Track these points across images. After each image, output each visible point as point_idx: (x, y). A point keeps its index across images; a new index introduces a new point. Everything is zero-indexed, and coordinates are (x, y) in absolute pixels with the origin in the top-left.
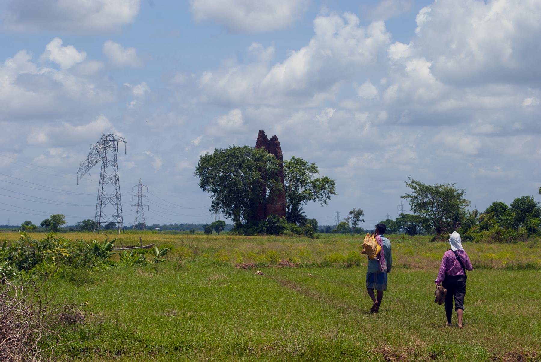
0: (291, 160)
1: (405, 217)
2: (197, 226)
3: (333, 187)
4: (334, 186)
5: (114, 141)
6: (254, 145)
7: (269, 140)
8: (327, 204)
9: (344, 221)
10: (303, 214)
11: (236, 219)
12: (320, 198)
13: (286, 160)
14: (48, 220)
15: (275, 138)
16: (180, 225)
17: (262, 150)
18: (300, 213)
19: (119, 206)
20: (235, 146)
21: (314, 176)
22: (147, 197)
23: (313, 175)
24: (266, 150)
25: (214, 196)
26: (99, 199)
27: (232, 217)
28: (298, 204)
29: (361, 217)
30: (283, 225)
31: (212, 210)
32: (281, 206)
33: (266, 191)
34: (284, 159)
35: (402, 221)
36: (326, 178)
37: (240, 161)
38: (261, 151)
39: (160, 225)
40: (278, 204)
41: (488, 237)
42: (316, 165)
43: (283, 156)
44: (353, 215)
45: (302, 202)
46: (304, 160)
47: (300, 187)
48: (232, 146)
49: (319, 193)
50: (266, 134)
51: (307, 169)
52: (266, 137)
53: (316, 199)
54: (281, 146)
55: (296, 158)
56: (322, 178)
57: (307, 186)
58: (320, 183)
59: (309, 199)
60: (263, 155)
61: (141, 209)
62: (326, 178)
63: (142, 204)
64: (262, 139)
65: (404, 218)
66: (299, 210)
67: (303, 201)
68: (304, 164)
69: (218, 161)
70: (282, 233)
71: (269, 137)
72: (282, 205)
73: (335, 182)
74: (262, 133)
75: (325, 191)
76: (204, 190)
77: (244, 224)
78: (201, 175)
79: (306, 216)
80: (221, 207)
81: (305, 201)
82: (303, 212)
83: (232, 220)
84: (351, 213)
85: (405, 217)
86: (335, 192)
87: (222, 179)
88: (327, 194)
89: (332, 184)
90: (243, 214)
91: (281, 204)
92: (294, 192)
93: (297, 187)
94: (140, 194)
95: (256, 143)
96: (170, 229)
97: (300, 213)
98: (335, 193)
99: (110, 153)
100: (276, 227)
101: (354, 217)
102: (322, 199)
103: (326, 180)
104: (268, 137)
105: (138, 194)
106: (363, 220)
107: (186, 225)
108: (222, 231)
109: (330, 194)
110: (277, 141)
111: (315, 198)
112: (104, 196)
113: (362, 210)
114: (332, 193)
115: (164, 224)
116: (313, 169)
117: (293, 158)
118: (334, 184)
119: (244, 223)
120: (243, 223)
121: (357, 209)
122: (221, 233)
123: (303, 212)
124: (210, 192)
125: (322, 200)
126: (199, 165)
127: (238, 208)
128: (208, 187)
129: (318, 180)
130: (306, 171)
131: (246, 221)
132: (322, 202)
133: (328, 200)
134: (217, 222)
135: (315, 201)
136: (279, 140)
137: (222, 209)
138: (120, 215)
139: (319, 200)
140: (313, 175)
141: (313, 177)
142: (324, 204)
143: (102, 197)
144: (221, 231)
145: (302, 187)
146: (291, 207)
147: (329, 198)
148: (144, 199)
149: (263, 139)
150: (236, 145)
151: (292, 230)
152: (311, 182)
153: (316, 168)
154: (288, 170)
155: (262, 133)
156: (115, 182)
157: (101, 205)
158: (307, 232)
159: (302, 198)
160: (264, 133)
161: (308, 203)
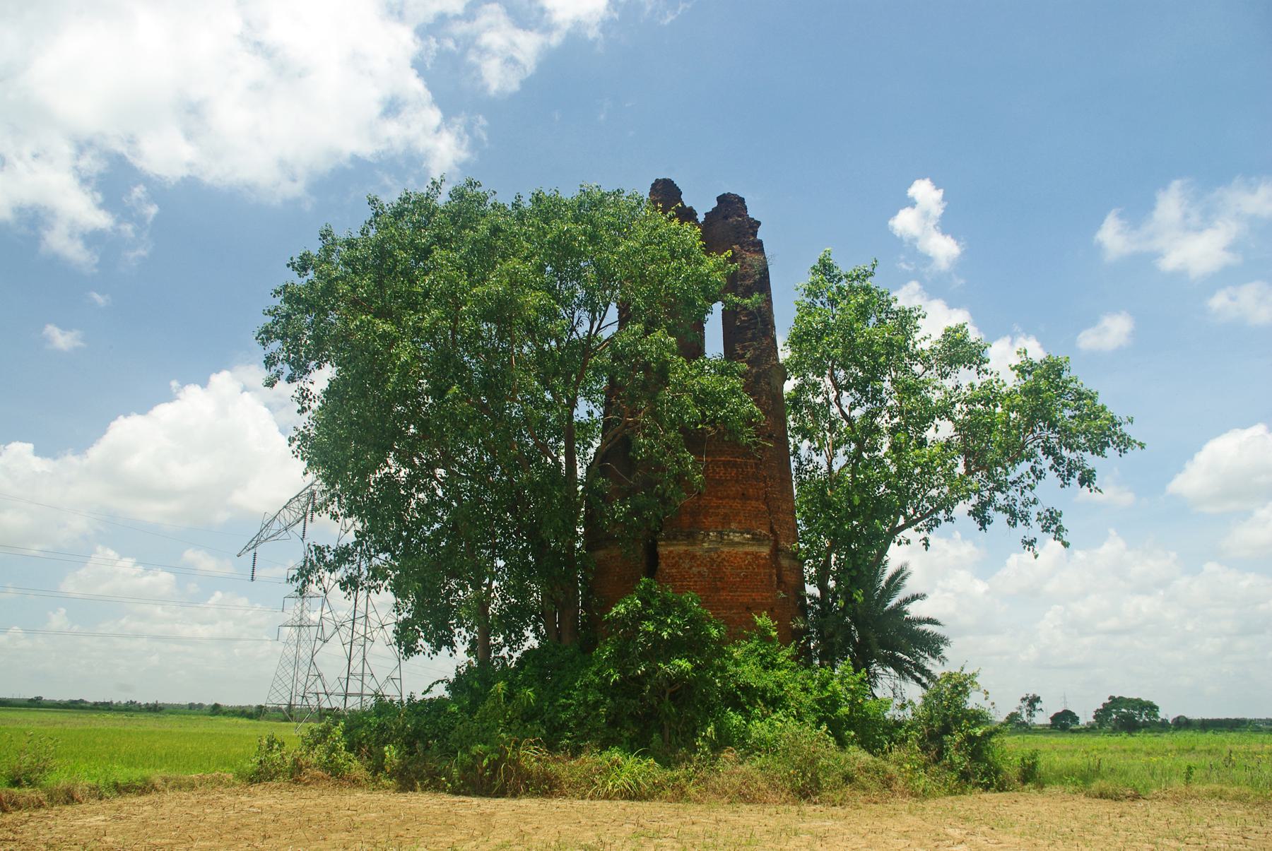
8: (1066, 545)
10: (914, 610)
18: (893, 602)
29: (1038, 706)
30: (459, 644)
32: (756, 556)
44: (1026, 703)
70: (723, 741)
72: (765, 551)
84: (1023, 700)
91: (757, 539)
97: (893, 602)
101: (1029, 705)
121: (1031, 695)
132: (1035, 529)
147: (1087, 479)
151: (826, 711)
158: (947, 730)
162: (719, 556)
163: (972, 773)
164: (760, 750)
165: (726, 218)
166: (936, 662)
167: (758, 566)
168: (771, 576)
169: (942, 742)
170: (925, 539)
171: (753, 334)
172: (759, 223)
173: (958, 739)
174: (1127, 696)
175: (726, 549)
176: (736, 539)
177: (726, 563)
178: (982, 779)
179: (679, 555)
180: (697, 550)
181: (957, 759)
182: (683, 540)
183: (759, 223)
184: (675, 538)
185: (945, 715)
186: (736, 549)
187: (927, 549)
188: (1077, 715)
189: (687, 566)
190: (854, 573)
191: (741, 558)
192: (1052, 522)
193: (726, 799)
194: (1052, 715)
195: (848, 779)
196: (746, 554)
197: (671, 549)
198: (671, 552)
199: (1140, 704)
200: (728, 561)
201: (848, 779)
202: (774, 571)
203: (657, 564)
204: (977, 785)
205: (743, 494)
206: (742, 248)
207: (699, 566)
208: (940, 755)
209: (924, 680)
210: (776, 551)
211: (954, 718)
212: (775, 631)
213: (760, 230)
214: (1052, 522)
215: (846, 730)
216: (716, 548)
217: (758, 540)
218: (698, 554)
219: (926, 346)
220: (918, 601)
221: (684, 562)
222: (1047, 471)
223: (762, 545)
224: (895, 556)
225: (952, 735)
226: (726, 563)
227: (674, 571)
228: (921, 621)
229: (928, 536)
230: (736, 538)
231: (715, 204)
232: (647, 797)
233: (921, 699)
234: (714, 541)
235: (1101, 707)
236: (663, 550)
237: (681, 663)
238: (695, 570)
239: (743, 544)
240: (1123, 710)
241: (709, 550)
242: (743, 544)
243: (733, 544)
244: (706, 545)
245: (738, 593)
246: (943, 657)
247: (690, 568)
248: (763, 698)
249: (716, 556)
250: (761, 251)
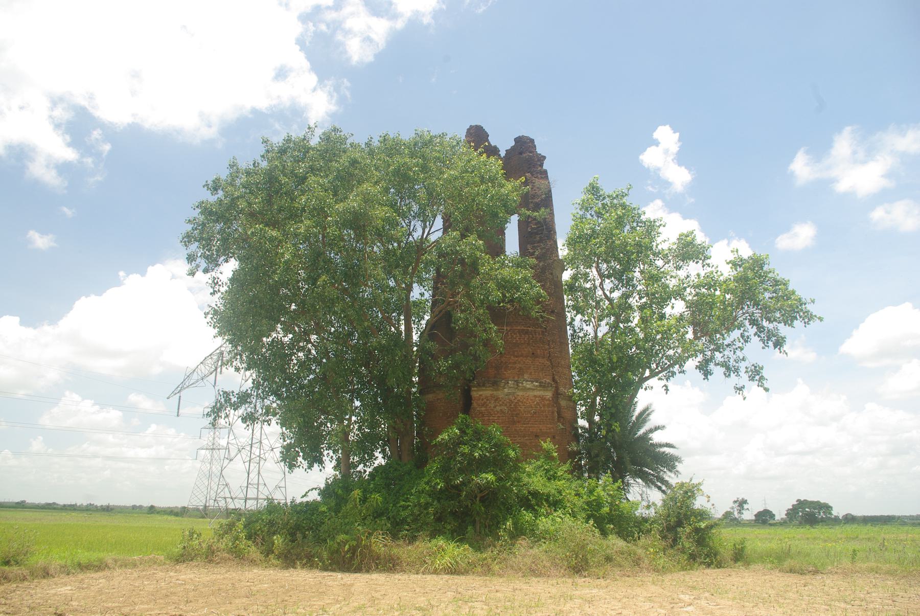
8: (767, 390)
9: (729, 510)
10: (657, 437)
16: (300, 503)
18: (641, 432)
29: (746, 506)
32: (543, 398)
41: (203, 461)
43: (552, 191)
44: (737, 504)
54: (546, 166)
72: (549, 394)
79: (668, 445)
84: (735, 502)
91: (543, 386)
97: (641, 432)
113: (746, 499)
121: (741, 499)
125: (743, 370)
131: (41, 438)
132: (744, 379)
158: (679, 524)
162: (516, 398)
163: (698, 555)
164: (545, 539)
165: (521, 153)
166: (672, 475)
167: (544, 405)
168: (553, 412)
169: (676, 533)
170: (665, 386)
171: (541, 237)
172: (544, 158)
173: (688, 530)
175: (520, 393)
176: (528, 386)
177: (520, 403)
178: (705, 559)
179: (486, 397)
180: (500, 394)
181: (687, 545)
182: (489, 387)
183: (544, 158)
184: (484, 386)
185: (679, 513)
186: (528, 393)
187: (667, 393)
189: (492, 406)
190: (613, 411)
191: (531, 400)
192: (756, 374)
193: (520, 574)
195: (609, 559)
196: (535, 396)
197: (481, 393)
198: (481, 395)
200: (522, 402)
201: (609, 559)
202: (556, 409)
203: (471, 404)
204: (701, 563)
205: (533, 354)
206: (532, 175)
207: (500, 405)
208: (675, 541)
209: (664, 488)
210: (557, 394)
211: (685, 515)
212: (556, 452)
213: (545, 162)
214: (756, 374)
215: (607, 524)
216: (514, 393)
217: (544, 387)
218: (500, 397)
219: (665, 246)
220: (659, 430)
221: (490, 403)
223: (547, 390)
224: (643, 399)
225: (684, 528)
226: (520, 403)
227: (483, 409)
228: (661, 445)
229: (667, 384)
231: (513, 144)
232: (465, 572)
233: (661, 502)
234: (511, 387)
235: (791, 507)
236: (475, 394)
237: (487, 476)
238: (498, 408)
239: (534, 390)
240: (807, 510)
242: (534, 390)
244: (506, 390)
245: (529, 425)
246: (677, 471)
247: (495, 407)
248: (547, 500)
249: (514, 398)
250: (546, 177)
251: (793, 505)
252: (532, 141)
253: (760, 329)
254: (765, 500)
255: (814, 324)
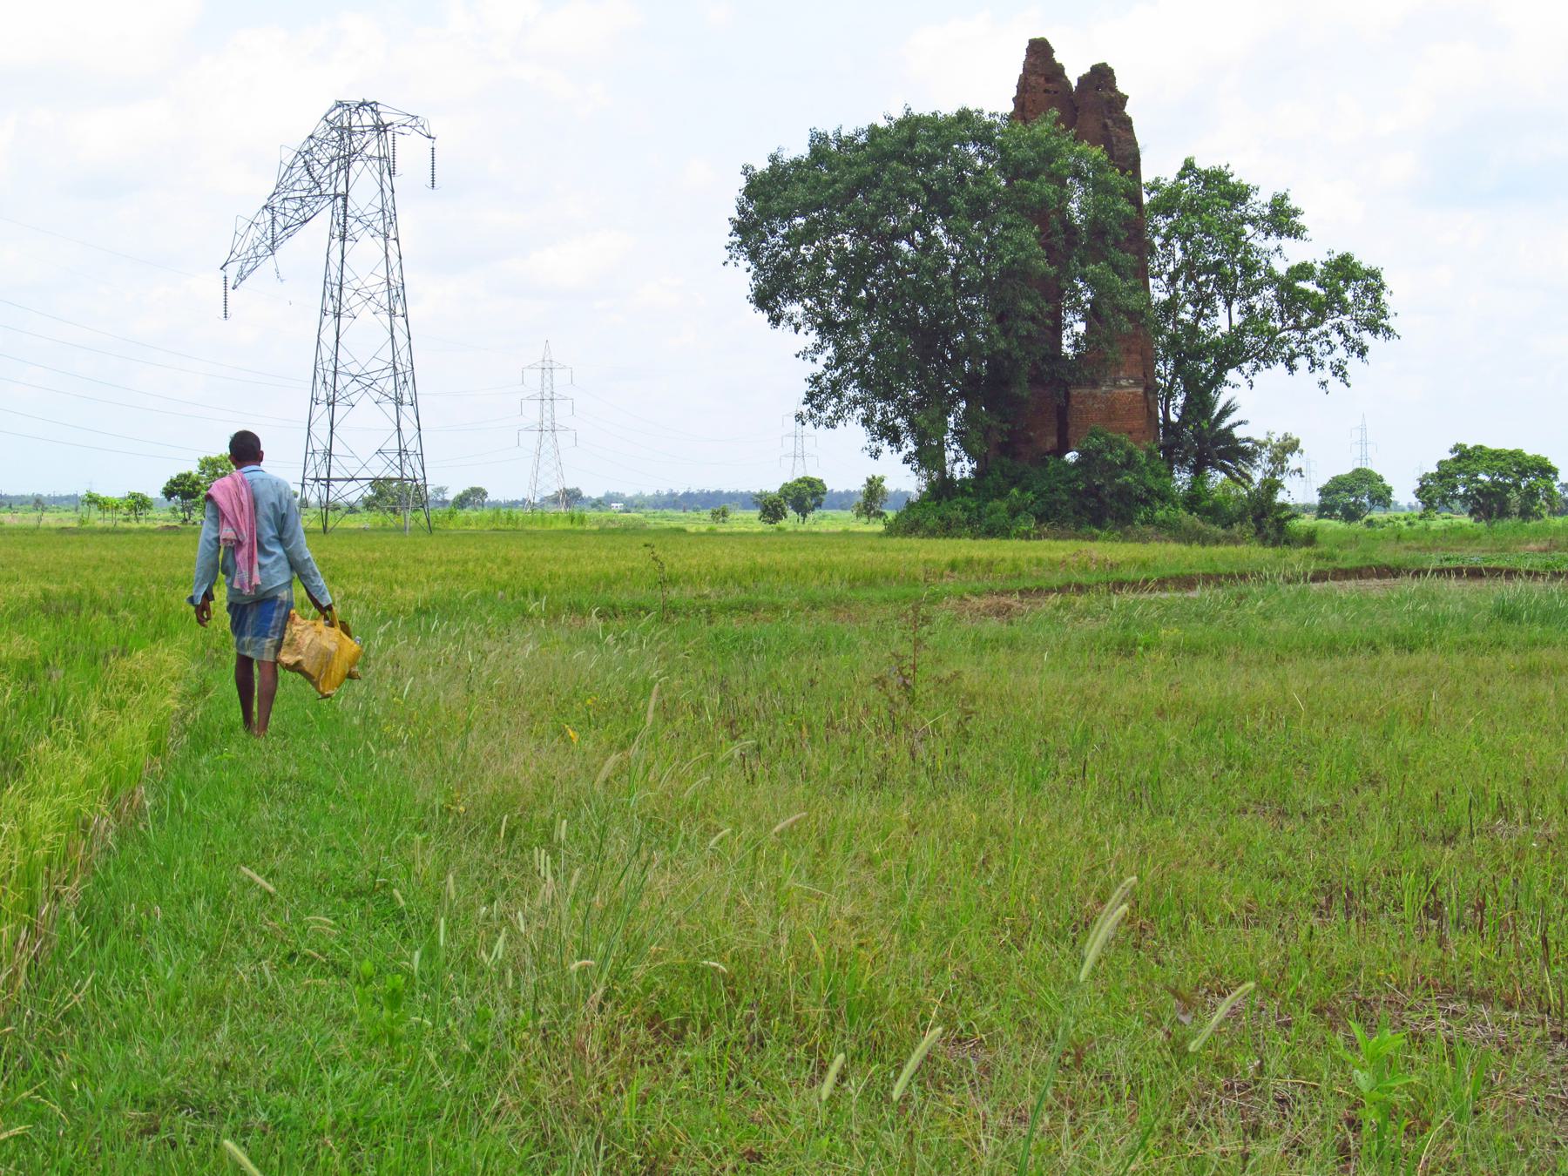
0: (1181, 176)
1: (1469, 457)
2: (732, 497)
3: (1377, 299)
4: (1384, 296)
5: (381, 128)
6: (1009, 108)
7: (1074, 83)
8: (1348, 385)
11: (927, 457)
12: (1318, 356)
13: (1157, 180)
14: (187, 476)
15: (1101, 76)
17: (1046, 125)
18: (1224, 426)
19: (407, 410)
20: (916, 112)
21: (1284, 251)
22: (570, 402)
23: (1278, 249)
24: (1068, 128)
25: (818, 349)
26: (319, 381)
27: (910, 446)
28: (1218, 380)
29: (1293, 461)
31: (811, 416)
32: (1135, 395)
33: (1057, 329)
34: (1147, 176)
35: (1461, 471)
36: (1345, 259)
37: (942, 178)
38: (1040, 129)
39: (627, 495)
40: (1124, 383)
42: (1292, 203)
45: (1232, 375)
46: (1240, 174)
47: (1220, 304)
48: (899, 115)
49: (1314, 332)
50: (1058, 57)
51: (1253, 221)
52: (1059, 70)
53: (1297, 361)
54: (1129, 110)
55: (1202, 164)
56: (1326, 258)
57: (1255, 298)
58: (1319, 285)
59: (1267, 358)
60: (1054, 149)
61: (551, 440)
62: (1345, 259)
63: (553, 424)
64: (1042, 80)
65: (1466, 462)
66: (1217, 411)
67: (1240, 369)
68: (1239, 195)
69: (835, 181)
71: (1074, 72)
72: (1140, 391)
73: (1385, 278)
74: (1039, 51)
75: (1345, 320)
76: (776, 320)
77: (963, 481)
78: (754, 256)
80: (855, 402)
81: (1247, 367)
82: (1240, 423)
83: (906, 461)
85: (1469, 457)
86: (1391, 322)
87: (855, 268)
88: (1352, 334)
89: (1372, 283)
90: (962, 437)
91: (1137, 384)
92: (1192, 330)
93: (1203, 302)
94: (547, 392)
95: (1014, 100)
96: (656, 507)
97: (1224, 426)
98: (1388, 330)
99: (364, 184)
100: (1124, 493)
102: (1327, 360)
103: (1343, 268)
104: (1067, 73)
105: (542, 393)
106: (1300, 471)
107: (701, 493)
108: (817, 511)
109: (1366, 337)
110: (1114, 89)
111: (1293, 356)
112: (343, 369)
113: (1295, 437)
114: (1376, 332)
115: (637, 493)
116: (1282, 219)
117: (1189, 166)
118: (1382, 286)
119: (966, 475)
120: (958, 477)
122: (810, 516)
123: (1240, 423)
124: (802, 330)
125: (1327, 366)
126: (742, 211)
127: (934, 401)
128: (795, 309)
129: (1303, 271)
130: (1248, 229)
132: (1326, 374)
133: (1353, 364)
134: (800, 481)
135: (1292, 369)
136: (1122, 86)
137: (860, 410)
138: (412, 447)
139: (1313, 363)
140: (1278, 249)
141: (1284, 255)
142: (1334, 383)
143: (335, 373)
144: (813, 510)
145: (1229, 304)
146: (1180, 400)
147: (1362, 352)
148: (562, 409)
149: (1048, 80)
150: (922, 109)
152: (1277, 279)
153: (1296, 212)
154: (1162, 223)
155: (1039, 51)
156: (387, 307)
157: (332, 404)
158: (1263, 515)
159: (1231, 353)
160: (1052, 51)
161: (1258, 378)
172: (1127, 97)
174: (1492, 444)
180: (1098, 392)
183: (1127, 97)
188: (1388, 482)
190: (1200, 406)
192: (1339, 370)
194: (1323, 481)
199: (1518, 464)
214: (1339, 370)
222: (1338, 346)
224: (1224, 396)
230: (1124, 383)
235: (1435, 470)
236: (1074, 392)
240: (1482, 477)
241: (1105, 392)
243: (1122, 387)
251: (1441, 464)
252: (1105, 65)
253: (1347, 338)
254: (1363, 429)
255: (1393, 341)
